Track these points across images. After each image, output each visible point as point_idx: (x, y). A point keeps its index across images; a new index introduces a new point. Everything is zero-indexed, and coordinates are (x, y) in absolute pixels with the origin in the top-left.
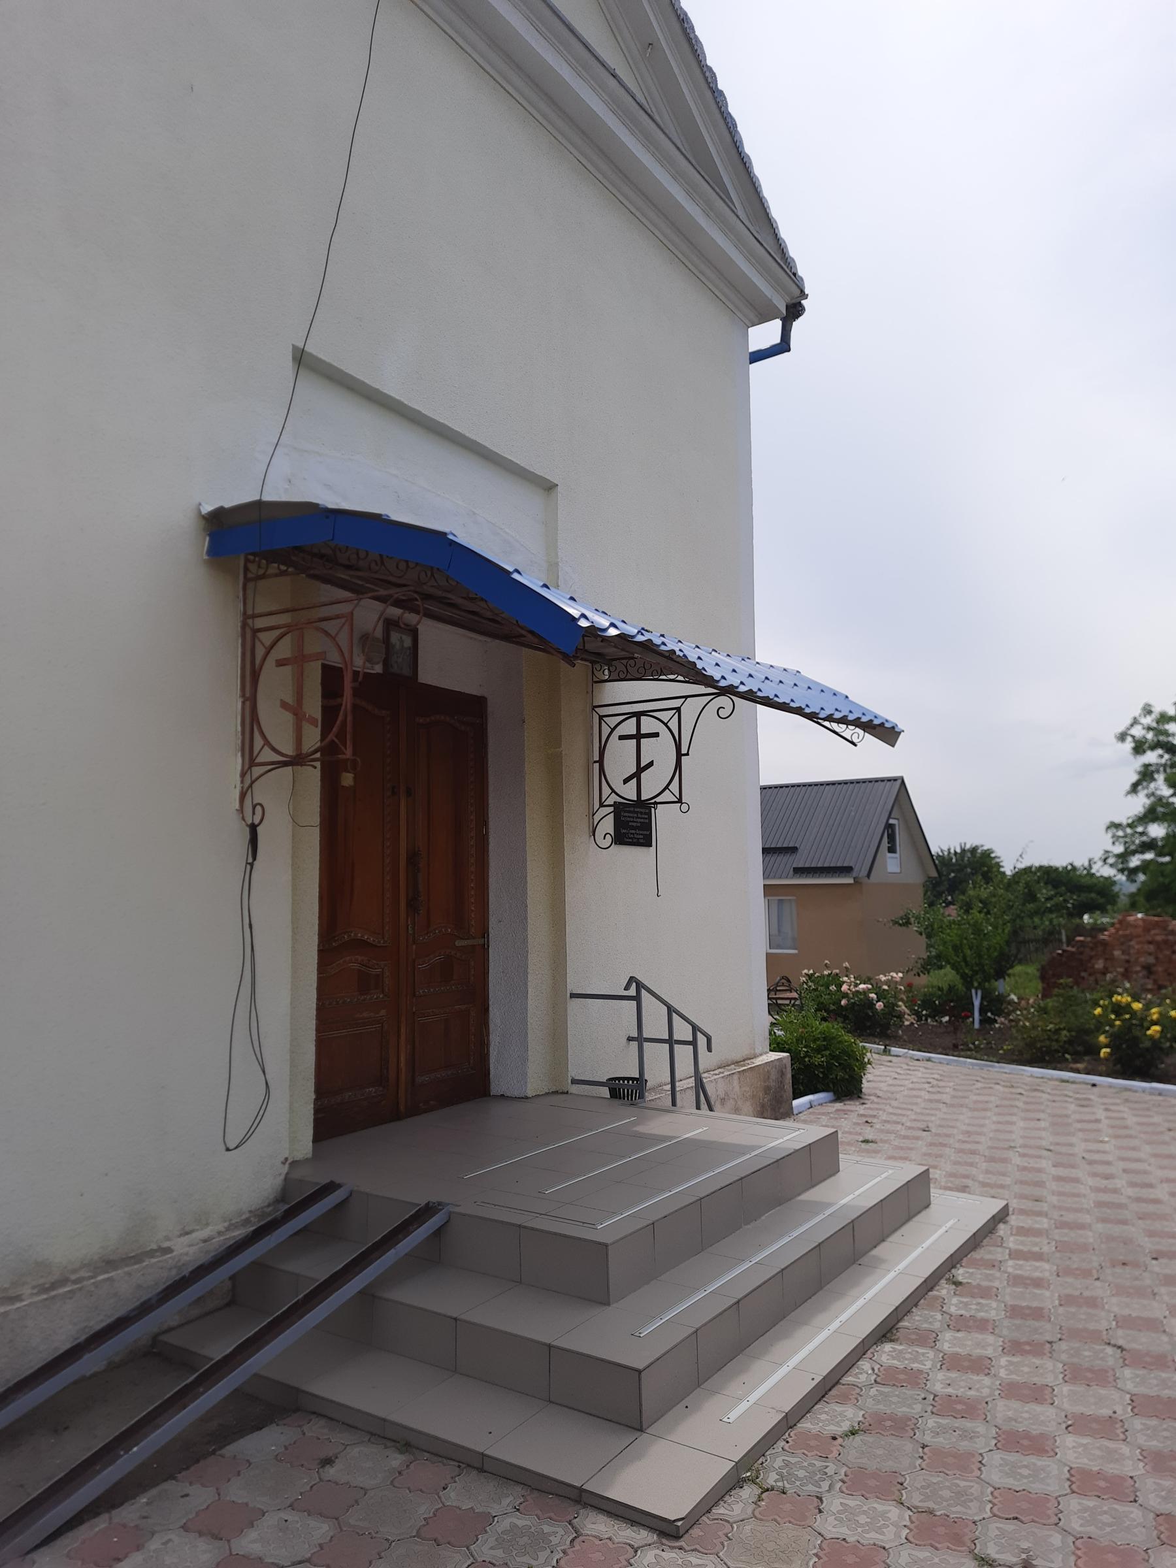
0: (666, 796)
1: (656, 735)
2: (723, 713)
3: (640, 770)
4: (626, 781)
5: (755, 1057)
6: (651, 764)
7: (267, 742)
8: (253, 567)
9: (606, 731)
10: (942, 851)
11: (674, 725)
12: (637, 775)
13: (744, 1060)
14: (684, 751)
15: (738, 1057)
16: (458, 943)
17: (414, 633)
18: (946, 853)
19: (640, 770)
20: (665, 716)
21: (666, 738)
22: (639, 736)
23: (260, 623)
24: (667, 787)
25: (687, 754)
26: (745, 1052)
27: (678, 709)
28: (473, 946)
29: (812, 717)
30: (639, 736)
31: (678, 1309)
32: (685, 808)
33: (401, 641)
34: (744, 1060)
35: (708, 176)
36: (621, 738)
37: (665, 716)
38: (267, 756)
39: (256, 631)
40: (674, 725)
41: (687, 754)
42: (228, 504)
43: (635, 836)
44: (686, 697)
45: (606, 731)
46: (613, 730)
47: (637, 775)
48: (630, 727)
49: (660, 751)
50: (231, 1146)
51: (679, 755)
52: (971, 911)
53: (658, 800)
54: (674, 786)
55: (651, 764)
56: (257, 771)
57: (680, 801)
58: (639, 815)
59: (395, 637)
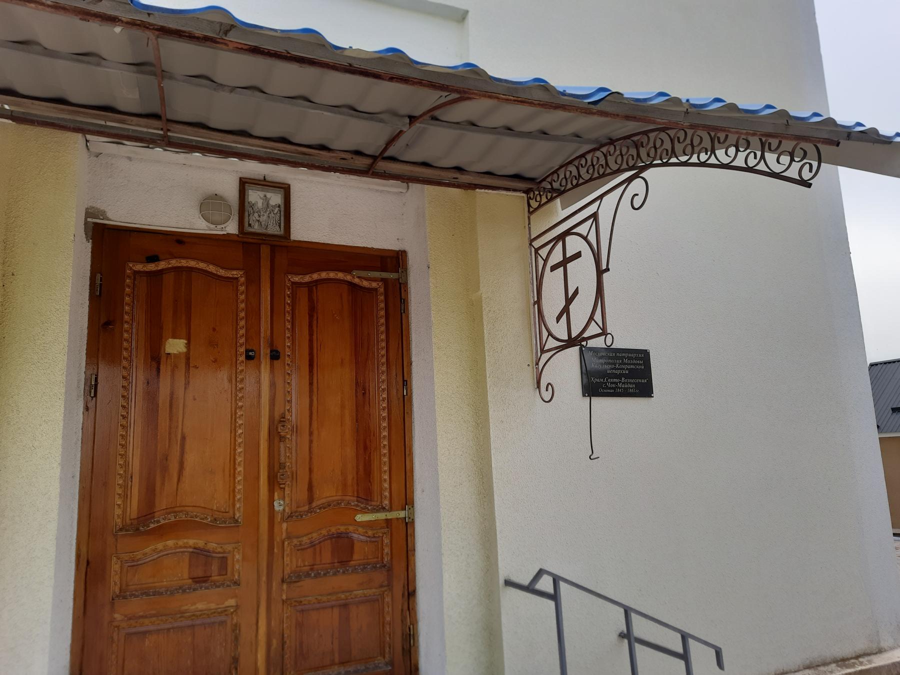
0: (593, 329)
1: (578, 255)
2: (637, 202)
3: (569, 300)
4: (558, 319)
5: (880, 651)
6: (576, 292)
7: (550, 334)
8: (533, 203)
11: (592, 238)
12: (566, 310)
13: (857, 657)
14: (604, 267)
15: (846, 650)
16: (360, 518)
17: (286, 190)
19: (569, 300)
20: (583, 229)
21: (588, 257)
23: (537, 244)
24: (591, 318)
25: (607, 270)
26: (861, 645)
27: (595, 216)
28: (388, 522)
33: (266, 199)
34: (857, 657)
37: (583, 229)
38: (552, 343)
39: (537, 250)
40: (592, 238)
41: (607, 270)
43: (620, 385)
47: (566, 310)
48: (557, 256)
51: (600, 272)
52: (289, 606)
53: (585, 335)
54: (598, 317)
55: (576, 292)
56: (546, 356)
58: (626, 361)
59: (255, 196)
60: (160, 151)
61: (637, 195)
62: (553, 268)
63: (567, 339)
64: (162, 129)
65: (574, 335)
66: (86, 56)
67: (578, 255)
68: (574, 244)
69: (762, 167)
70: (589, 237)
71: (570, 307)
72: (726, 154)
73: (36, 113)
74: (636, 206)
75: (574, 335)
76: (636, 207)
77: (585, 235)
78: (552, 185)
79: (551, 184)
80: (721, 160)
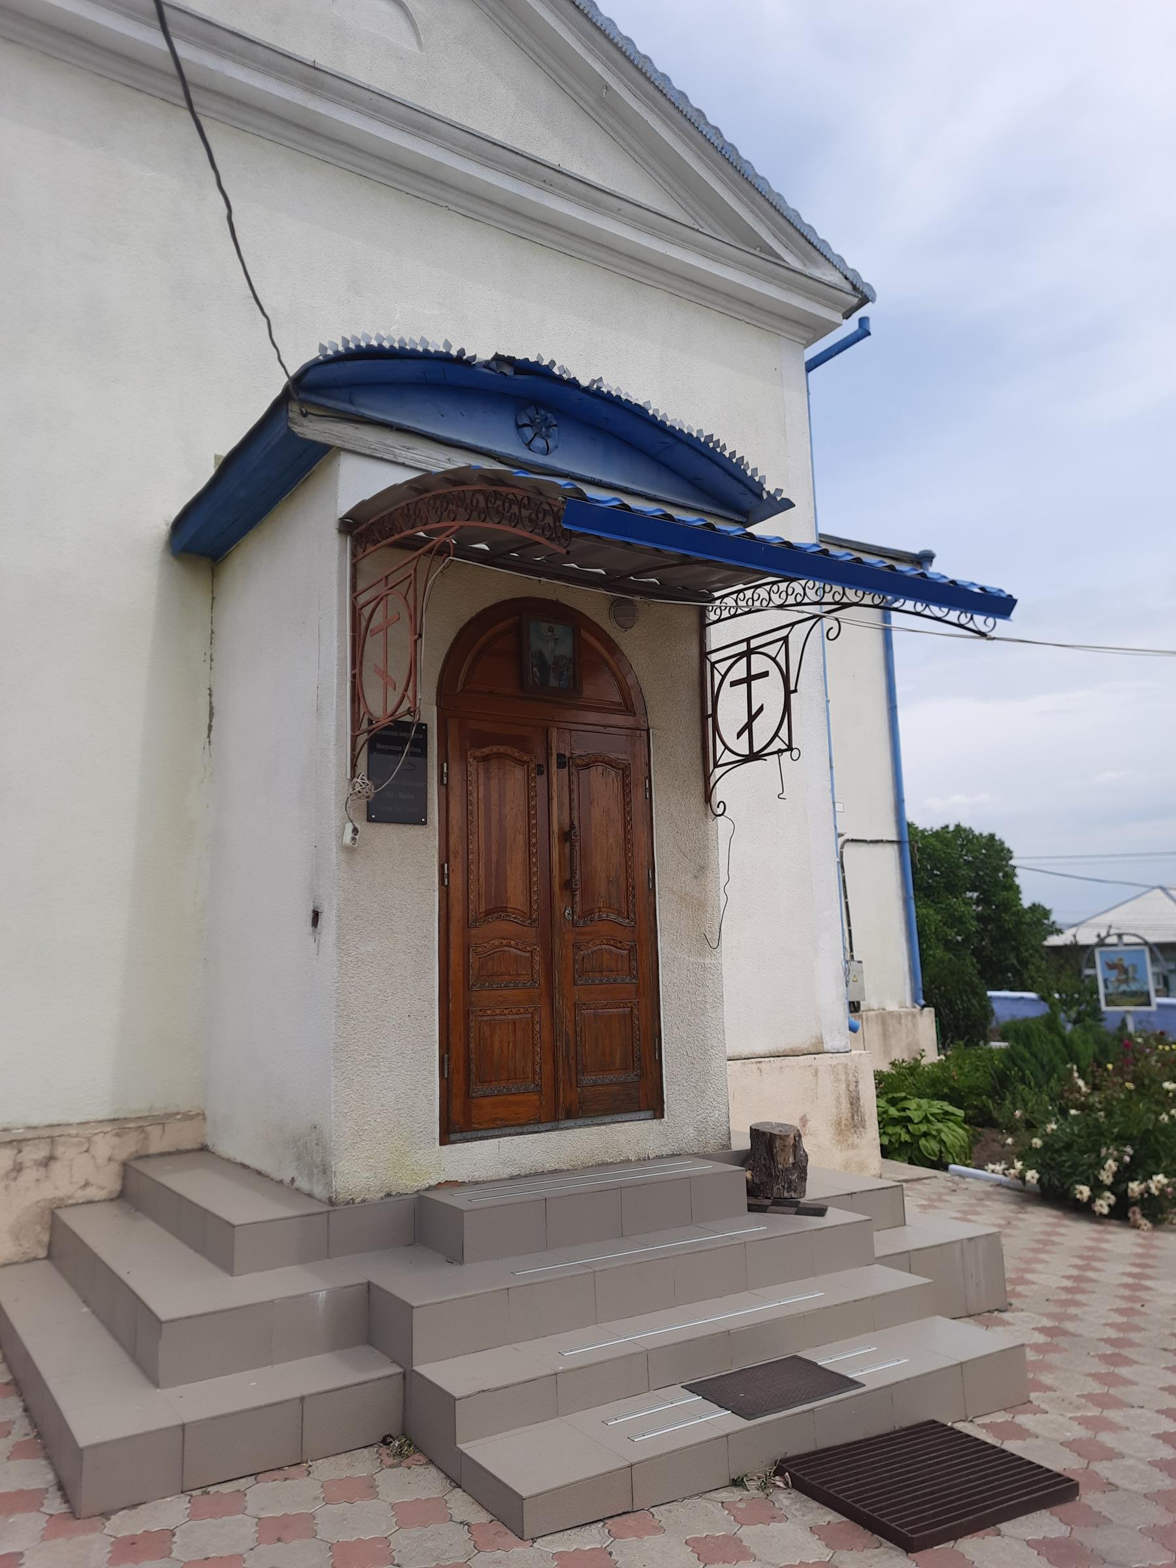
0: (777, 745)
1: (765, 674)
2: (832, 635)
3: (752, 717)
4: (739, 735)
6: (761, 709)
9: (718, 678)
10: (700, 431)
11: (781, 660)
12: (748, 727)
14: (792, 688)
18: (727, 454)
19: (752, 717)
20: (772, 650)
21: (775, 676)
22: (749, 679)
24: (776, 735)
27: (785, 640)
29: (484, 1391)
30: (749, 679)
31: (856, 1351)
32: (795, 753)
35: (1006, 998)
36: (733, 684)
37: (772, 650)
40: (781, 660)
41: (795, 691)
42: (367, 497)
44: (793, 625)
45: (718, 678)
46: (724, 677)
47: (748, 727)
48: (739, 672)
49: (768, 692)
50: (794, 759)
51: (788, 693)
55: (761, 709)
57: (790, 748)
60: (823, 1360)
61: (832, 628)
62: (733, 684)
63: (748, 753)
64: (626, 753)
65: (755, 750)
66: (972, 1276)
67: (765, 674)
68: (759, 663)
69: (971, 625)
70: (777, 659)
71: (747, 720)
72: (856, 594)
73: (582, 473)
74: (831, 637)
75: (755, 750)
76: (831, 637)
77: (774, 656)
78: (737, 604)
79: (736, 601)
80: (977, 625)
